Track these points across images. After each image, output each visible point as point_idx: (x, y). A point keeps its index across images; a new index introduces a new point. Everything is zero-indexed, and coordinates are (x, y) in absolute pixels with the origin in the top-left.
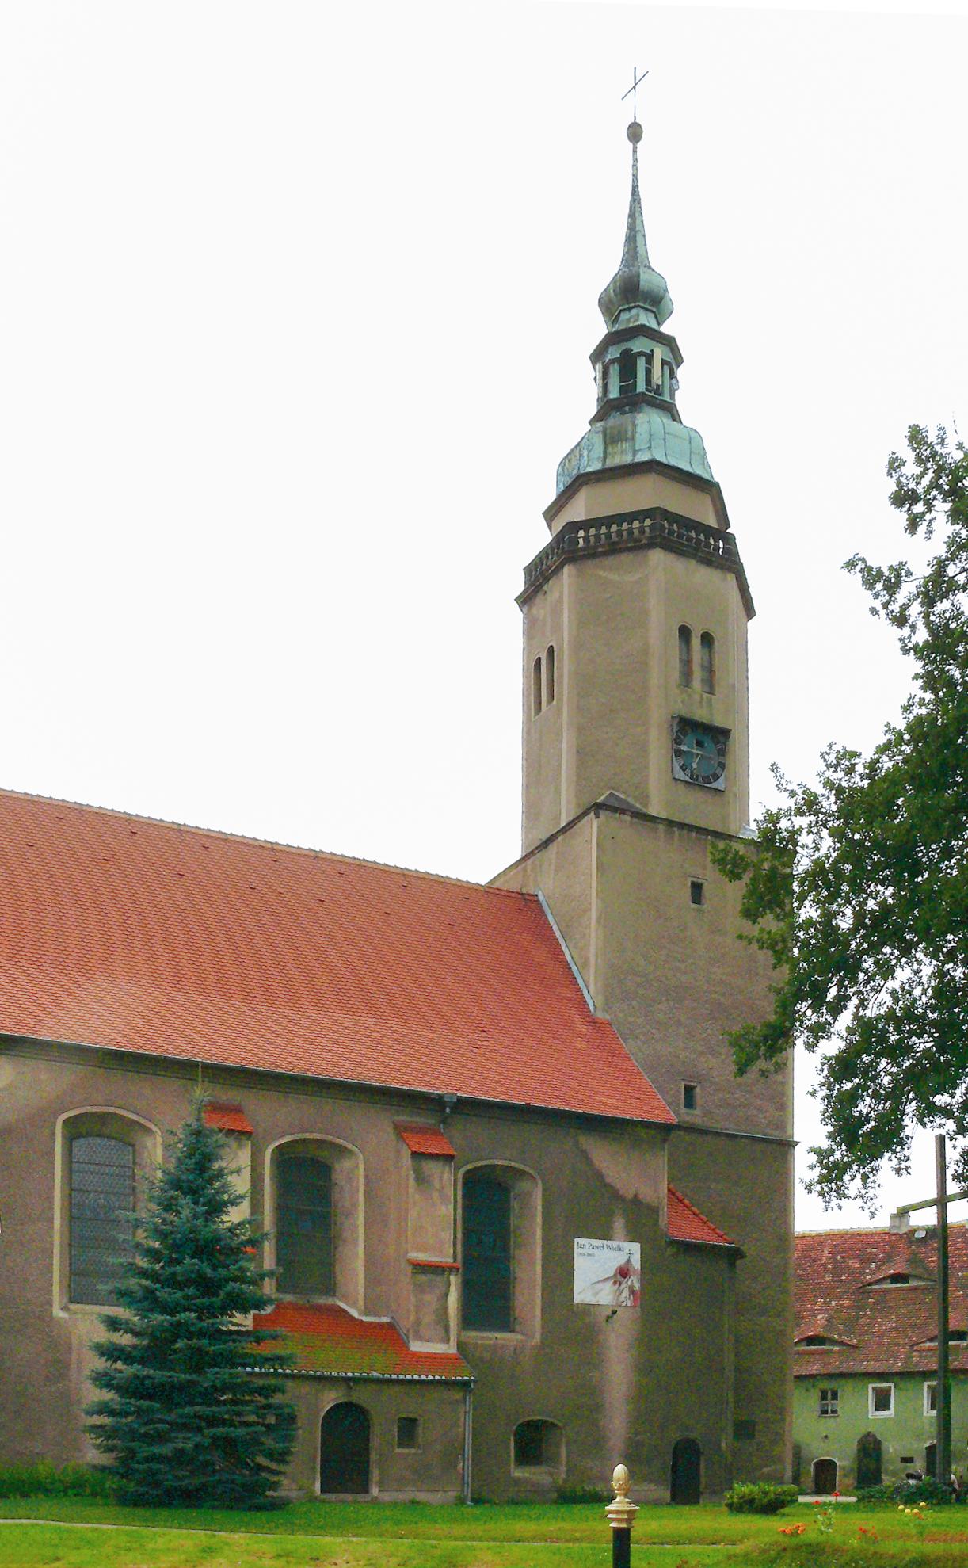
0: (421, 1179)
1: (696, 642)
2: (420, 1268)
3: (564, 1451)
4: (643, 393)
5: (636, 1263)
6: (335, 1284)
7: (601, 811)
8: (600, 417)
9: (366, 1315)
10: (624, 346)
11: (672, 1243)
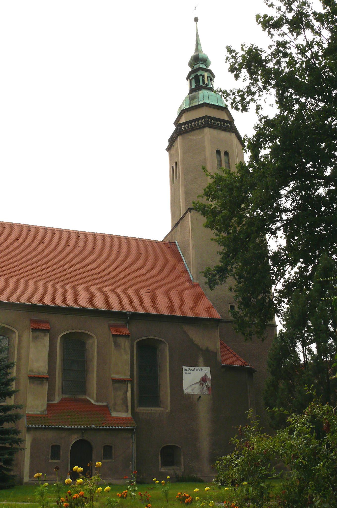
0: (117, 345)
1: (222, 155)
2: (116, 381)
3: (182, 458)
4: (202, 86)
5: (209, 376)
6: (86, 390)
7: (192, 211)
8: (189, 94)
9: (97, 402)
10: (195, 74)
11: (223, 367)
